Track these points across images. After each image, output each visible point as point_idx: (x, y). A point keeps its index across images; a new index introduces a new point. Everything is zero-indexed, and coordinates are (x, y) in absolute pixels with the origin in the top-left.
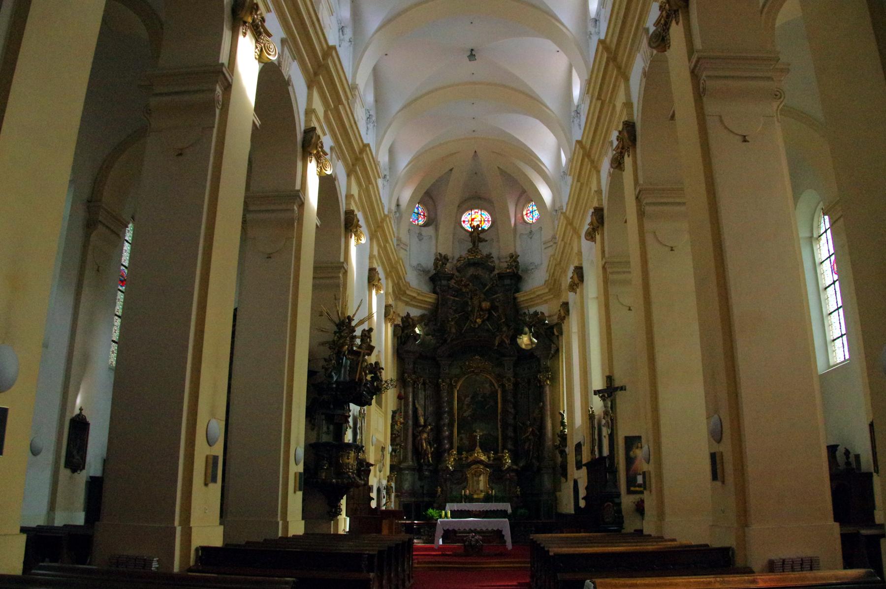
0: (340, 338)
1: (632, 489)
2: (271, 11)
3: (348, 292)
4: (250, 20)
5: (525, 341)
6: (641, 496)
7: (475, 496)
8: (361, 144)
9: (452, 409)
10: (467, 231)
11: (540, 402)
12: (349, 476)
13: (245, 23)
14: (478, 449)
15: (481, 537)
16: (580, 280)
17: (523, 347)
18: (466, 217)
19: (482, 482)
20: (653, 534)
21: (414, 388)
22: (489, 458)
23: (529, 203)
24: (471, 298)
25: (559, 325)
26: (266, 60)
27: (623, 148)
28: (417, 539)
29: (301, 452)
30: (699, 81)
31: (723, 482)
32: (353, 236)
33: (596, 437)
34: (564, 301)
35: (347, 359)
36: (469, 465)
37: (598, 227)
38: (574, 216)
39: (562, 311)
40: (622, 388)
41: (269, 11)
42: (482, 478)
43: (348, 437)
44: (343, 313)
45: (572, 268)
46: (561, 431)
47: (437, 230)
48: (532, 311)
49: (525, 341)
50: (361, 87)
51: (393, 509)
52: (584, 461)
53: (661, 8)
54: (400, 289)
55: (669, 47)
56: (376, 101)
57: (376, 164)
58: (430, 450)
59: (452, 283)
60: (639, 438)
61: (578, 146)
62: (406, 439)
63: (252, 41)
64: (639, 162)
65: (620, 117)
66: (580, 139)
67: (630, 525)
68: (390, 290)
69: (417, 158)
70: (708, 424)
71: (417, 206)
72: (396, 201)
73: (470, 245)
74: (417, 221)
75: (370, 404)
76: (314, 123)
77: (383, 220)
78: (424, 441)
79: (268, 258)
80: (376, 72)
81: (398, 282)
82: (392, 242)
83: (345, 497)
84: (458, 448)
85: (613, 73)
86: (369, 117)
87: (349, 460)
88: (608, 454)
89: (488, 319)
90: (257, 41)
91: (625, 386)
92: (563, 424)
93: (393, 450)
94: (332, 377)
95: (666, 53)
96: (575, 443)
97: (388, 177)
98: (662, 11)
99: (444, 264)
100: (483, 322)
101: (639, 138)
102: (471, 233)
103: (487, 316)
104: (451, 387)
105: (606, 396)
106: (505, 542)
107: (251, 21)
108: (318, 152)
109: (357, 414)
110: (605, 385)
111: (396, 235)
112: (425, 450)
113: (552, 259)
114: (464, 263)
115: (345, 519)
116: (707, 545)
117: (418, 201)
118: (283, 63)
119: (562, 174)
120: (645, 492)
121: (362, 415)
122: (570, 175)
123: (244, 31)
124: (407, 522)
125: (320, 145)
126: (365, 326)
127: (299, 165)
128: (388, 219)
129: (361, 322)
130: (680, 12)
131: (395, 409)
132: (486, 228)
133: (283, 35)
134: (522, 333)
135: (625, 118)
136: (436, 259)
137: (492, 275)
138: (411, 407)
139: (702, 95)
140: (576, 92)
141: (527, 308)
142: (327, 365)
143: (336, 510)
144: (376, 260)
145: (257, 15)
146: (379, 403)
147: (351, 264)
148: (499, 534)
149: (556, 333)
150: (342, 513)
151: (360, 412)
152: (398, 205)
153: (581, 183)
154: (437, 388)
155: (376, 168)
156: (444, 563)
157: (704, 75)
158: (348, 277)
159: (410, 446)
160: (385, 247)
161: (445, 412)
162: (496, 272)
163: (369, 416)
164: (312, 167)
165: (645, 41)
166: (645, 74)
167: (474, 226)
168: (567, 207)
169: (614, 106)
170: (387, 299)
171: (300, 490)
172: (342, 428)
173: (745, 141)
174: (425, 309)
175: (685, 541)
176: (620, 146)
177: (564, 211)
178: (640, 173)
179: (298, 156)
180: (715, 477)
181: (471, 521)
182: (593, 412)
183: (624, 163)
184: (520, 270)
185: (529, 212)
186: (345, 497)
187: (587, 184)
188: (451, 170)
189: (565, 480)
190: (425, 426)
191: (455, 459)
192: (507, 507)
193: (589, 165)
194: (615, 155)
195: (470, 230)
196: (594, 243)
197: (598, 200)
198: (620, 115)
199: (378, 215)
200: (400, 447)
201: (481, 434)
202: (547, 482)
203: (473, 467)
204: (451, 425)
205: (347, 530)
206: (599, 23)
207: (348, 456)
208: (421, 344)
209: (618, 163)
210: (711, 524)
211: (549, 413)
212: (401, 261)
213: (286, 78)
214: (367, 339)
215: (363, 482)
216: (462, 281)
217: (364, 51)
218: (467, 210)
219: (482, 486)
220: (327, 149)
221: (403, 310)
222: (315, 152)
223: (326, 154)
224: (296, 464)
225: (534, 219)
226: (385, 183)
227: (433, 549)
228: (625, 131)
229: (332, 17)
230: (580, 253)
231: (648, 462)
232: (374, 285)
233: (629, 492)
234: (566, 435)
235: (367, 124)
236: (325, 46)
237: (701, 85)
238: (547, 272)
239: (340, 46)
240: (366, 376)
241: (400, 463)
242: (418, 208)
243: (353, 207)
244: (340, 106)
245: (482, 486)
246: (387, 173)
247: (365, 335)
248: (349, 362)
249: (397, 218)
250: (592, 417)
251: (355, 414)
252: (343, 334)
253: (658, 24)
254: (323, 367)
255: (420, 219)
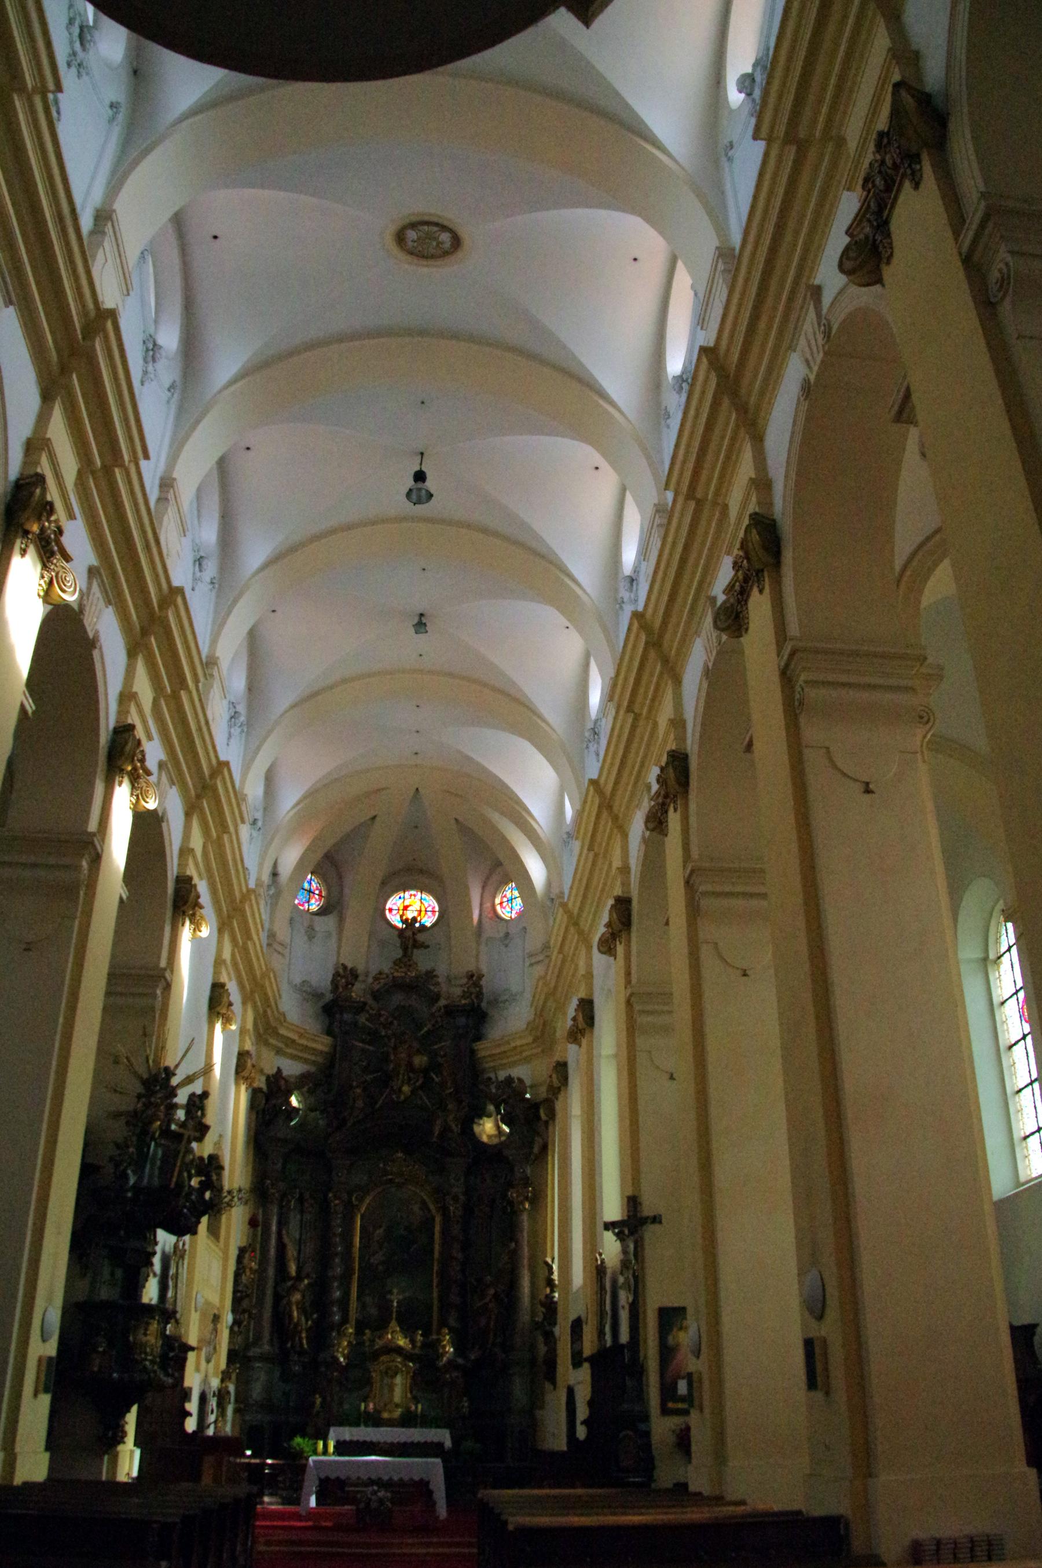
0: (147, 1106)
1: (670, 1405)
2: (75, 519)
3: (171, 1023)
4: (35, 528)
5: (488, 1128)
6: (686, 1418)
7: (385, 1415)
8: (214, 761)
9: (349, 1245)
10: (395, 927)
11: (512, 1239)
12: (145, 1367)
13: (26, 533)
14: (394, 1325)
15: (389, 1495)
16: (587, 1024)
17: (485, 1139)
18: (394, 902)
19: (399, 1387)
20: (706, 1491)
21: (281, 1207)
22: (413, 1341)
23: (507, 884)
24: (395, 1048)
25: (549, 1104)
26: (56, 600)
27: (666, 796)
28: (271, 1495)
29: (55, 1317)
30: (793, 687)
31: (827, 1393)
32: (188, 923)
33: (608, 1307)
34: (560, 1060)
35: (156, 1145)
36: (376, 1356)
37: (620, 931)
38: (581, 909)
39: (554, 1076)
40: (656, 1219)
41: (72, 516)
42: (398, 1380)
43: (150, 1293)
44: (157, 1061)
45: (574, 1003)
46: (547, 1296)
47: (341, 920)
48: (502, 1075)
49: (488, 1128)
50: (224, 663)
51: (230, 1434)
52: (587, 1352)
53: (736, 566)
54: (268, 1023)
55: (747, 630)
56: (251, 688)
57: (240, 798)
58: (306, 1324)
59: (362, 1019)
60: (683, 1310)
61: (591, 788)
62: (260, 1302)
63: (35, 565)
64: (693, 820)
65: (665, 742)
66: (595, 776)
67: (665, 1476)
68: (250, 1025)
69: (311, 795)
70: (801, 1283)
71: (309, 876)
72: (272, 863)
73: (398, 953)
74: (306, 905)
75: (194, 1232)
76: (134, 718)
77: (246, 897)
78: (294, 1308)
79: (25, 950)
80: (253, 638)
81: (265, 1012)
82: (259, 937)
83: (135, 1409)
84: (358, 1321)
85: (655, 667)
86: (234, 716)
87: (148, 1338)
88: (628, 1340)
89: (421, 1087)
90: (45, 567)
91: (660, 1216)
92: (550, 1283)
93: (236, 1322)
94: (126, 1177)
95: (742, 639)
96: (573, 1317)
97: (260, 824)
98: (737, 571)
99: (349, 984)
100: (412, 1092)
101: (694, 783)
102: (401, 932)
103: (420, 1082)
104: (350, 1211)
105: (626, 1232)
106: (434, 1504)
107: (38, 532)
108: (135, 769)
109: (169, 1249)
110: (626, 1213)
111: (267, 926)
112: (297, 1325)
113: (541, 984)
114: (385, 984)
115: (132, 1452)
116: (799, 1513)
117: (311, 868)
118: (87, 609)
119: (565, 836)
120: (692, 1411)
121: (179, 1253)
122: (577, 838)
123: (23, 546)
124: (253, 1461)
125: (140, 756)
126: (197, 1088)
127: (99, 788)
128: (253, 897)
129: (189, 1080)
130: (766, 574)
131: (244, 1244)
132: (428, 924)
133: (92, 560)
134: (482, 1113)
135: (671, 745)
136: (337, 975)
137: (434, 1010)
138: (273, 1242)
139: (798, 712)
140: (595, 697)
141: (495, 1069)
142: (120, 1155)
143: (115, 1435)
144: (227, 969)
145: (50, 522)
146: (214, 1231)
147: (180, 976)
148: (422, 1488)
149: (543, 1116)
150: (126, 1439)
151: (176, 1246)
152: (275, 874)
153: (564, 956)
154: (325, 1209)
155: (239, 805)
156: (318, 1543)
157: (802, 678)
158: (172, 996)
159: (267, 1314)
160: (245, 949)
161: (336, 1254)
162: (442, 1002)
163: (193, 1257)
164: (122, 796)
165: (709, 619)
166: (707, 673)
167: (407, 919)
168: (570, 892)
169: (655, 725)
170: (242, 1041)
171: (46, 1390)
172: (139, 1273)
173: (868, 791)
174: (314, 1063)
175: (761, 1507)
176: (663, 793)
177: (566, 900)
178: (694, 839)
179: (99, 770)
180: (812, 1383)
181: (372, 1462)
182: (603, 1261)
183: (667, 821)
184: (485, 1000)
185: (505, 899)
186: (135, 1409)
187: (605, 857)
188: (374, 818)
189: (552, 1387)
190: (299, 1278)
191: (349, 1343)
192: (444, 1437)
193: (610, 823)
194: (653, 806)
195: (400, 925)
196: (612, 958)
197: (623, 884)
198: (665, 741)
199: (236, 887)
200: (250, 1317)
201: (401, 1297)
202: (519, 1391)
203: (383, 1358)
204: (346, 1278)
205: (135, 1473)
206: (637, 584)
207: (146, 1329)
208: (301, 1125)
209: (657, 822)
210: (808, 1472)
211: (526, 1262)
212: (272, 975)
213: (91, 635)
214: (197, 1112)
215: (170, 1381)
216: (380, 1015)
217: (235, 601)
218: (396, 890)
219: (398, 1395)
220: (151, 764)
221: (271, 1062)
222: (129, 768)
223: (148, 773)
224: (44, 1340)
225: (514, 912)
226: (255, 834)
227: (297, 1516)
228: (671, 767)
229: (183, 539)
230: (589, 976)
231: (697, 1354)
232: (219, 1013)
233: (665, 1411)
234: (556, 1303)
235: (230, 727)
236: (165, 586)
237: (797, 696)
238: (531, 1006)
239: (193, 589)
240: (190, 1180)
241: (247, 1347)
242: (310, 883)
243: (191, 871)
244: (182, 692)
245: (398, 1395)
246: (259, 815)
247: (194, 1105)
248: (160, 1152)
249: (271, 897)
250: (600, 1270)
251: (167, 1249)
252: (153, 1100)
253: (730, 591)
254: (111, 1159)
255: (313, 901)
